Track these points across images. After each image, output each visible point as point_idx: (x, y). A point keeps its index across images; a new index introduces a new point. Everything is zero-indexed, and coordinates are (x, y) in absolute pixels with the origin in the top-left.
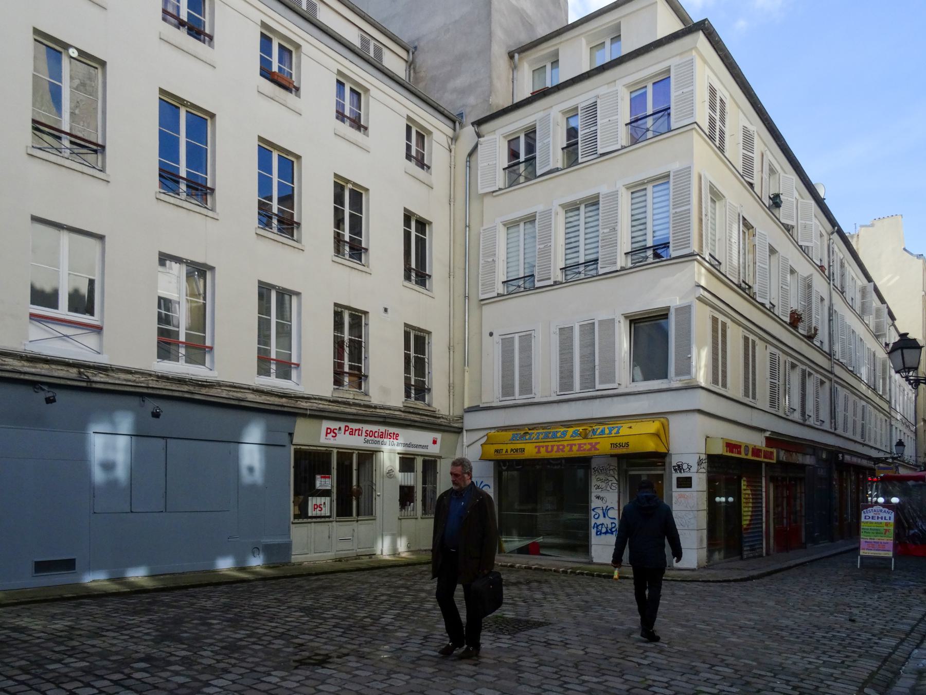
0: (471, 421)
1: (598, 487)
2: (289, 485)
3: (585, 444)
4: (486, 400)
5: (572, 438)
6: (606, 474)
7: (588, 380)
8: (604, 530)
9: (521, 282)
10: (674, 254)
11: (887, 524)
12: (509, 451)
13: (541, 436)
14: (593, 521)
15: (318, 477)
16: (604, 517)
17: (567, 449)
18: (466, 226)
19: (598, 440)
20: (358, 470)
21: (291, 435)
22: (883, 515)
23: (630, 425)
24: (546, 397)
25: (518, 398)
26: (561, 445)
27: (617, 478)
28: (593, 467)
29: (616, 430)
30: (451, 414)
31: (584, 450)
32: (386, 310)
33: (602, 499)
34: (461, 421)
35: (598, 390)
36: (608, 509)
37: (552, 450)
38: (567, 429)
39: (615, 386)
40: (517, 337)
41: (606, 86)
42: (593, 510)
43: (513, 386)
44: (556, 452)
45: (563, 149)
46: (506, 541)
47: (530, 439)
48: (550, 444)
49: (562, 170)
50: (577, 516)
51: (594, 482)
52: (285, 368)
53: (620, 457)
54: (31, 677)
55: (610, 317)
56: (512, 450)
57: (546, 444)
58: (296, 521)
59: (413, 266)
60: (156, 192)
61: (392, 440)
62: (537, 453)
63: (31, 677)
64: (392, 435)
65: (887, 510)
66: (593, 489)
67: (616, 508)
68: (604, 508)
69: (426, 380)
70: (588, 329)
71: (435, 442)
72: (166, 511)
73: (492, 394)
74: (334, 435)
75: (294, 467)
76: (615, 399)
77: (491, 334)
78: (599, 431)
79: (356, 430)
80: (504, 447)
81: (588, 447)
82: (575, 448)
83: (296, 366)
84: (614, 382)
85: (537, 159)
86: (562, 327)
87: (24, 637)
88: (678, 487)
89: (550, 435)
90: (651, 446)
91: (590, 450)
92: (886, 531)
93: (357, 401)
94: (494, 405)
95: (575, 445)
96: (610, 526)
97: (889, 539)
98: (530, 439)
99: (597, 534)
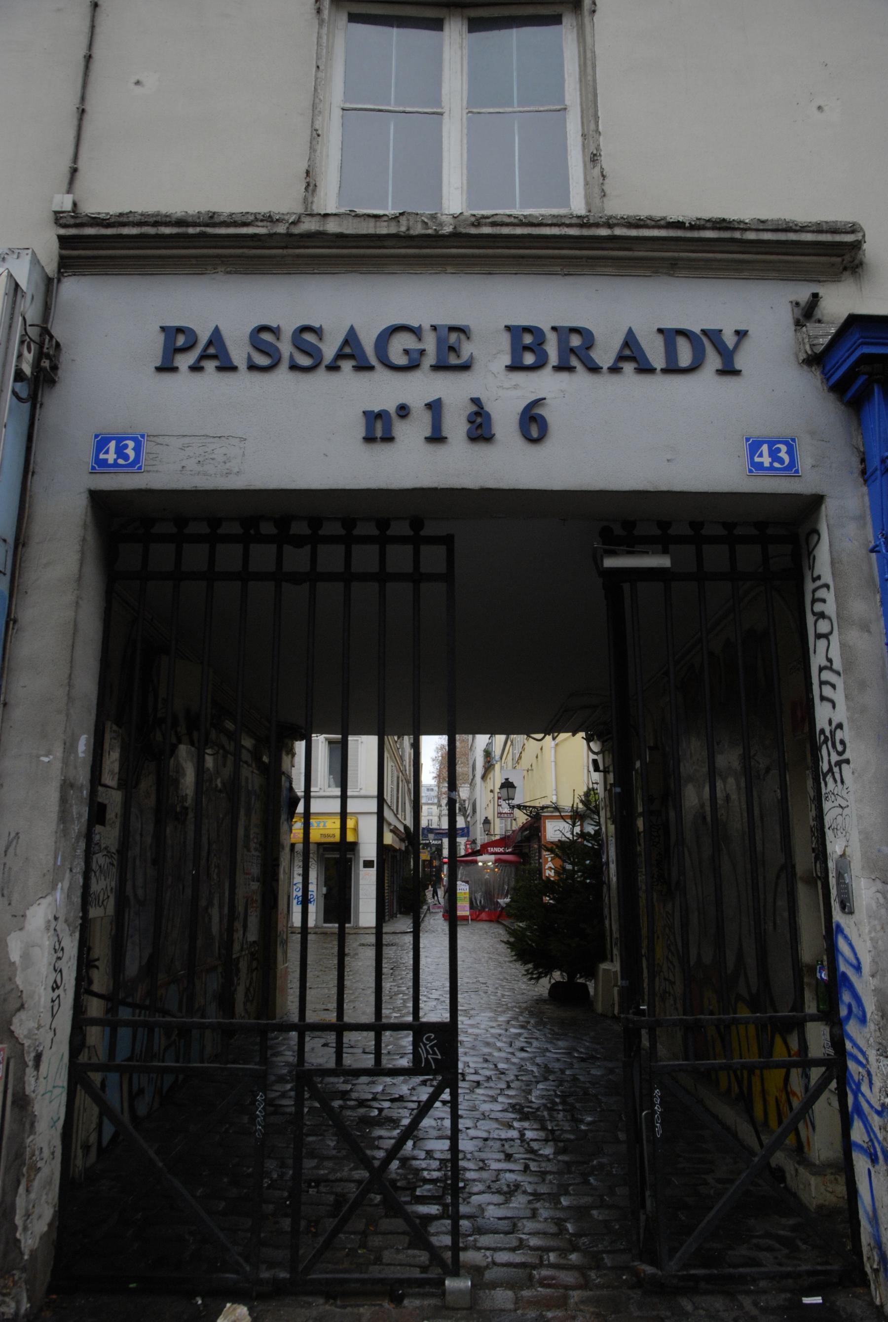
11: (465, 893)
23: (333, 821)
27: (316, 859)
29: (322, 824)
54: (860, 1095)
63: (860, 1095)
87: (27, 1126)
92: (465, 898)
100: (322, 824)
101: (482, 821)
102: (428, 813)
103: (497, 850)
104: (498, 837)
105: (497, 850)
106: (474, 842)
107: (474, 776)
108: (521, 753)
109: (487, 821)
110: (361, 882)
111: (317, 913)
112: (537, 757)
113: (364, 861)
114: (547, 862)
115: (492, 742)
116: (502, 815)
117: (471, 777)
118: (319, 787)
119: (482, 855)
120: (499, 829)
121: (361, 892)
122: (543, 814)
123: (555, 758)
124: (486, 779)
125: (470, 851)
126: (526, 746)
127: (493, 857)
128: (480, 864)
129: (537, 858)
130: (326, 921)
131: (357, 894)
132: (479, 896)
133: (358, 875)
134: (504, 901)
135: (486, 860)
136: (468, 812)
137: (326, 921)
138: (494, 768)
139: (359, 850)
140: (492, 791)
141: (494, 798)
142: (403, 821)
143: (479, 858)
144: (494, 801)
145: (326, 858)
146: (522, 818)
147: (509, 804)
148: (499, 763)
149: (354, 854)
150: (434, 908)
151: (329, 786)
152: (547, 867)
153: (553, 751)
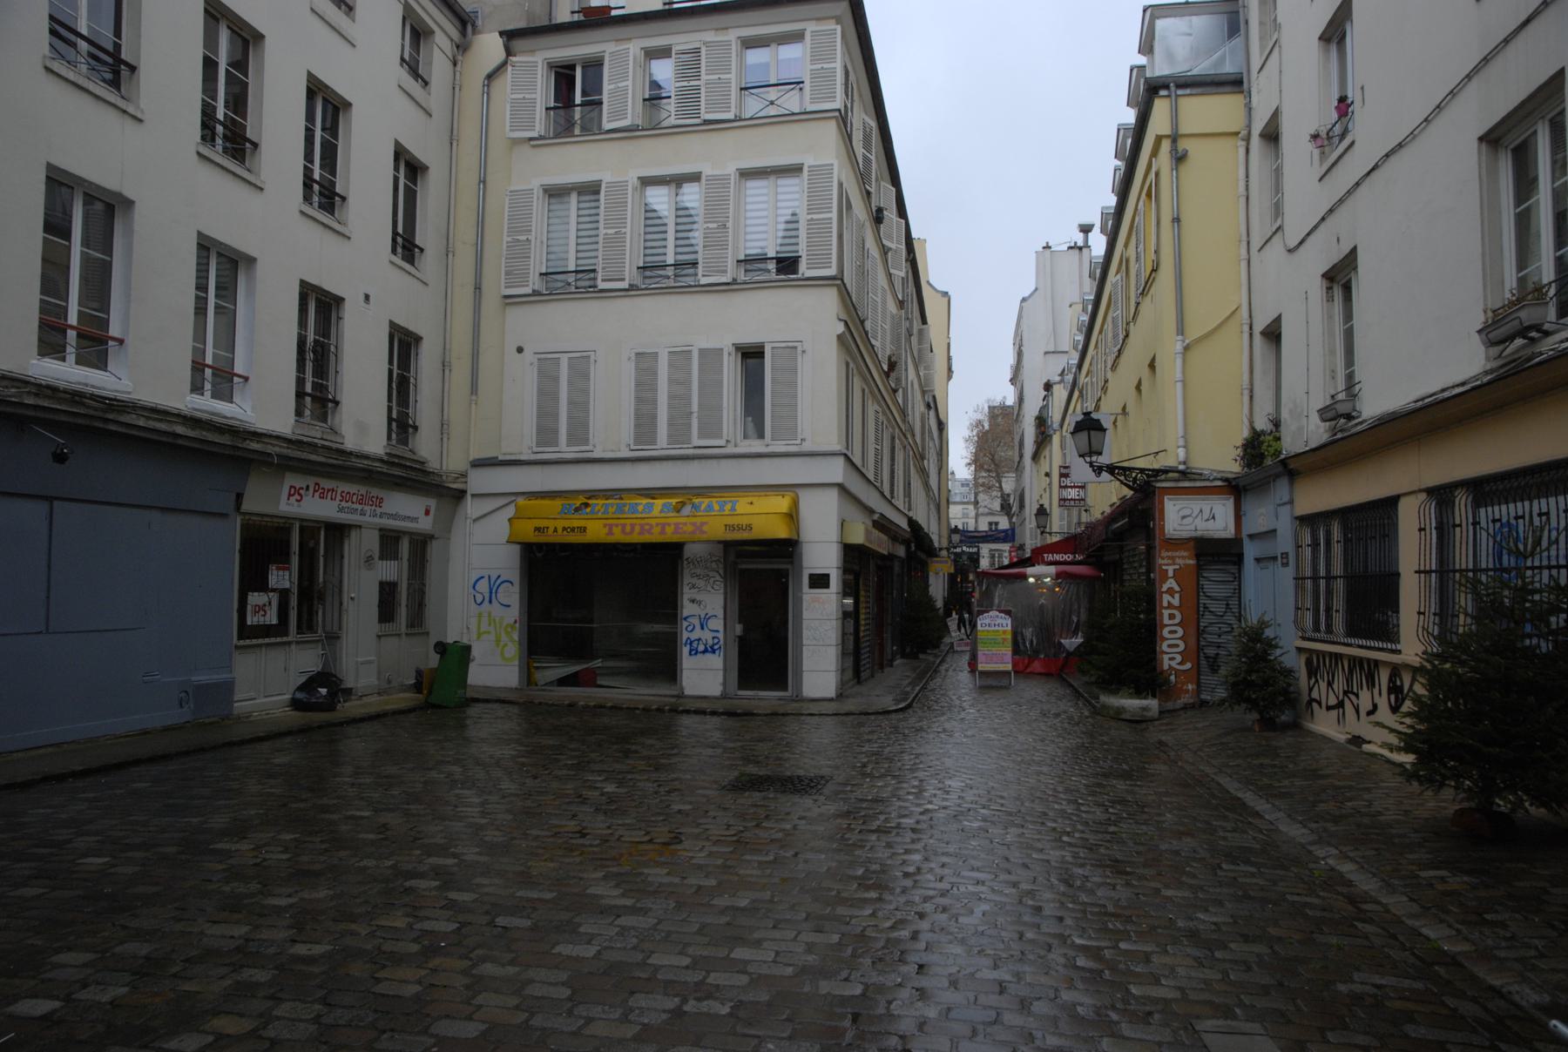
0: (479, 481)
1: (693, 586)
2: (232, 583)
3: (685, 524)
4: (506, 451)
5: (663, 515)
6: (707, 568)
7: (679, 431)
8: (701, 648)
9: (571, 278)
10: (704, 281)
11: (1005, 632)
12: (560, 530)
13: (611, 510)
14: (685, 635)
15: (273, 567)
16: (702, 628)
17: (656, 530)
18: (480, 182)
19: (705, 519)
20: (325, 556)
21: (239, 497)
22: (999, 621)
23: (750, 499)
24: (613, 451)
25: (565, 450)
26: (648, 524)
27: (721, 572)
28: (685, 557)
29: (728, 507)
30: (444, 468)
31: (685, 532)
32: (367, 297)
33: (700, 603)
34: (463, 480)
35: (695, 447)
36: (707, 618)
37: (633, 530)
38: (652, 501)
39: (722, 442)
40: (564, 359)
41: (713, 32)
42: (685, 619)
43: (556, 432)
44: (640, 534)
45: (1479, 332)
46: (537, 668)
47: (592, 512)
48: (628, 522)
49: (643, 130)
50: (658, 627)
51: (687, 579)
52: (225, 380)
53: (727, 545)
55: (718, 347)
56: (564, 529)
57: (622, 521)
58: (242, 643)
59: (400, 230)
60: (45, 57)
61: (373, 508)
62: (608, 534)
64: (374, 500)
65: (1003, 615)
66: (686, 589)
67: (722, 616)
68: (702, 616)
69: (410, 411)
70: (680, 357)
71: (427, 513)
72: (47, 632)
73: (522, 441)
74: (299, 498)
75: (240, 551)
76: (724, 462)
77: (520, 350)
78: (703, 506)
79: (329, 490)
80: (551, 524)
81: (690, 528)
82: (669, 530)
83: (241, 380)
84: (722, 438)
85: (605, 107)
86: (641, 351)
88: (811, 587)
89: (627, 509)
90: (781, 532)
91: (693, 532)
92: (1004, 639)
93: (326, 443)
94: (523, 458)
95: (669, 524)
96: (710, 642)
97: (1007, 651)
98: (592, 512)
99: (690, 654)
100: (728, 507)
101: (1035, 512)
102: (964, 514)
103: (1057, 557)
104: (1056, 539)
105: (1057, 557)
106: (1021, 547)
107: (1021, 456)
108: (1099, 400)
109: (1042, 512)
110: (806, 615)
111: (725, 670)
112: (1138, 387)
113: (811, 576)
114: (1165, 577)
115: (1047, 405)
116: (1067, 503)
117: (1017, 459)
118: (725, 437)
119: (1034, 565)
120: (1060, 524)
121: (805, 633)
122: (1158, 485)
123: (1184, 372)
124: (1039, 458)
125: (1015, 560)
126: (1110, 385)
127: (1052, 569)
128: (1031, 580)
129: (1143, 570)
130: (742, 686)
131: (799, 636)
132: (1028, 633)
133: (799, 601)
134: (1072, 642)
135: (1041, 575)
136: (1014, 509)
137: (742, 686)
138: (1050, 441)
139: (801, 554)
140: (1047, 475)
141: (1050, 484)
142: (906, 512)
143: (1030, 570)
144: (1051, 489)
145: (743, 572)
146: (1106, 496)
147: (1091, 464)
148: (1058, 433)
149: (792, 563)
150: (959, 645)
151: (746, 437)
152: (1164, 589)
153: (1179, 362)
